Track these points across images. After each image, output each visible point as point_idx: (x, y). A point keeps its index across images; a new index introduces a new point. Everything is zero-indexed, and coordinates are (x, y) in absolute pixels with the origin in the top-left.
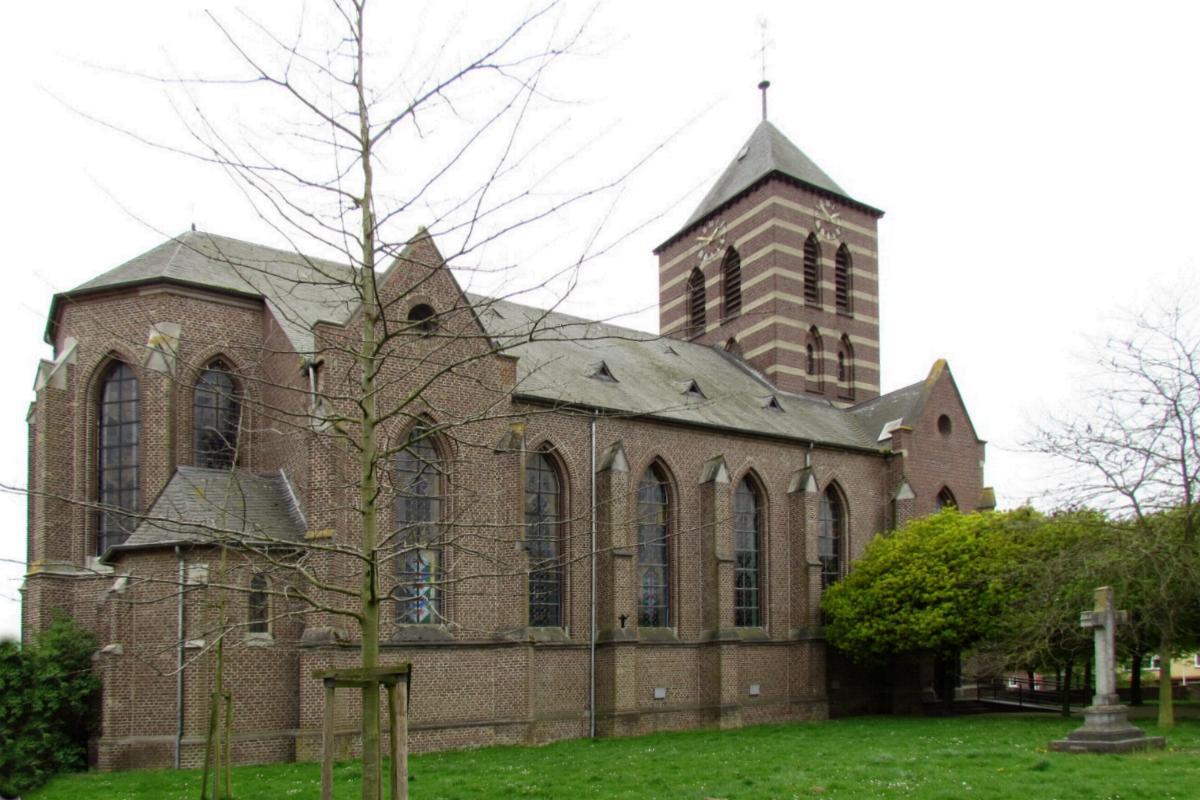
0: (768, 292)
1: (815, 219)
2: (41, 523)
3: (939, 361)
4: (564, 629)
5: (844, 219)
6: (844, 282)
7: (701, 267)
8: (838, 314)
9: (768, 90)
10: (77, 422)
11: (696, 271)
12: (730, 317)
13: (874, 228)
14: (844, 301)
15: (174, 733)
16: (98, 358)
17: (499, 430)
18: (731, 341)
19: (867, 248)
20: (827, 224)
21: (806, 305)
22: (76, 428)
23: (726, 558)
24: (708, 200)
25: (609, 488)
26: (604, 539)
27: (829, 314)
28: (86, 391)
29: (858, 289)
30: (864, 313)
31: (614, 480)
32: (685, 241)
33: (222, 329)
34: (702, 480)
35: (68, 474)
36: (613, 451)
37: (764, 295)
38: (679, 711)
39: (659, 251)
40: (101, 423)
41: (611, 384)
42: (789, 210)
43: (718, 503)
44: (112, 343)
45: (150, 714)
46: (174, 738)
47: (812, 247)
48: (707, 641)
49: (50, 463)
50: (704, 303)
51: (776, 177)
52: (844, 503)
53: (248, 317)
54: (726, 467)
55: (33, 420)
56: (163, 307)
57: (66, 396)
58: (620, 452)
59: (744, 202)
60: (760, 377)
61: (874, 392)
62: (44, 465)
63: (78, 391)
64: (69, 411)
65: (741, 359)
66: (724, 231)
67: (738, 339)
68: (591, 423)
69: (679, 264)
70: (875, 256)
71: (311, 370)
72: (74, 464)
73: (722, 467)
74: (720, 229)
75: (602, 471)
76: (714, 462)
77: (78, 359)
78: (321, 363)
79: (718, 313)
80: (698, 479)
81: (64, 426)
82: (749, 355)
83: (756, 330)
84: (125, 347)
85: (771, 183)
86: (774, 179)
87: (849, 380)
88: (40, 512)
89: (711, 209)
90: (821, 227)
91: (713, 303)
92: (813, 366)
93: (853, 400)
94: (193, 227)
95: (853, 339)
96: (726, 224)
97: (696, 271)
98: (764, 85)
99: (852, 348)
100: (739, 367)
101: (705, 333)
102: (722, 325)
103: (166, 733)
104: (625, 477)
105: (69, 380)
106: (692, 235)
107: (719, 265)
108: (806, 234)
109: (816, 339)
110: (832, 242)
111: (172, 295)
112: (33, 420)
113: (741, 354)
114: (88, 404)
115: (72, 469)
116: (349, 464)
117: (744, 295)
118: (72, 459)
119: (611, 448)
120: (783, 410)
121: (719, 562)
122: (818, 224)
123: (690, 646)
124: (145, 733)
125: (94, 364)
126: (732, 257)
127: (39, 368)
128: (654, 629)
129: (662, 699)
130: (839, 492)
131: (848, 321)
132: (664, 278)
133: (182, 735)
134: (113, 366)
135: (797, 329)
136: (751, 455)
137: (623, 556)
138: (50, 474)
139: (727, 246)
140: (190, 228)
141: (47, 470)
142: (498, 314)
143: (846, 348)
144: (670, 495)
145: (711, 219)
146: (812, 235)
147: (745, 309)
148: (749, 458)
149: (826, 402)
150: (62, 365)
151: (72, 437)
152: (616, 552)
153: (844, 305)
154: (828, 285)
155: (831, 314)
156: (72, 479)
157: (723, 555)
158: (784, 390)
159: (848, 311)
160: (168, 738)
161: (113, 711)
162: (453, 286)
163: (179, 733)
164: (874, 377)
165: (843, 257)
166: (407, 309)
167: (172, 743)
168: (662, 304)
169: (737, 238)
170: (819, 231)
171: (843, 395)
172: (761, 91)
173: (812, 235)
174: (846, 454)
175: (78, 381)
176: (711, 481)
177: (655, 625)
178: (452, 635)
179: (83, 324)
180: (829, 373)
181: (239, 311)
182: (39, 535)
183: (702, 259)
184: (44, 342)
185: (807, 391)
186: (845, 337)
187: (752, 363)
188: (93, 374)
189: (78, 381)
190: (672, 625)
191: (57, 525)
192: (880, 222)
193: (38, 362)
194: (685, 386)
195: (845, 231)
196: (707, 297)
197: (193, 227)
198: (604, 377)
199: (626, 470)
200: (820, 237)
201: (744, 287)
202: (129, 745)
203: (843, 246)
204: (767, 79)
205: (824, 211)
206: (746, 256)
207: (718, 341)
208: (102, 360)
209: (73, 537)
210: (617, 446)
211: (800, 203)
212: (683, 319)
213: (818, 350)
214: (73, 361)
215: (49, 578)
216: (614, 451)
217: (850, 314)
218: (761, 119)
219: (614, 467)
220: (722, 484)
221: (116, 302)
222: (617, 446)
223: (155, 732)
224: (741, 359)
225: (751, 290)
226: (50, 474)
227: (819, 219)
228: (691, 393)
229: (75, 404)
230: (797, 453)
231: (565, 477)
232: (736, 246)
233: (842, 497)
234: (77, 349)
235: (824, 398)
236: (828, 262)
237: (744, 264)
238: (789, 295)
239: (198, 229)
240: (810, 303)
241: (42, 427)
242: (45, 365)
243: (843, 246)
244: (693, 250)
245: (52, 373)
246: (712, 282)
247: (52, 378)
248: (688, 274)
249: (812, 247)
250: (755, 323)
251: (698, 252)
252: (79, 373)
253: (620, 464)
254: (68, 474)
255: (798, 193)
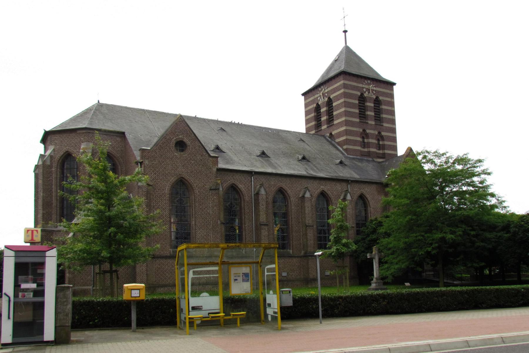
0: (343, 117)
1: (363, 88)
2: (41, 212)
3: (409, 147)
4: (243, 250)
5: (377, 87)
6: (378, 111)
7: (319, 103)
8: (375, 124)
9: (347, 33)
10: (54, 176)
11: (318, 104)
12: (331, 124)
13: (392, 90)
14: (378, 118)
15: (91, 285)
16: (62, 154)
17: (212, 182)
18: (331, 134)
19: (389, 97)
20: (368, 90)
21: (360, 122)
22: (53, 178)
23: (309, 225)
24: (323, 76)
25: (258, 200)
26: (257, 220)
27: (371, 125)
28: (58, 165)
29: (385, 114)
30: (388, 123)
31: (260, 198)
32: (313, 92)
33: (107, 145)
34: (300, 196)
35: (51, 194)
36: (260, 187)
37: (341, 118)
38: (293, 281)
39: (303, 94)
40: (63, 176)
41: (266, 158)
42: (350, 85)
43: (306, 204)
44: (65, 149)
45: (82, 279)
46: (91, 287)
47: (362, 99)
48: (304, 255)
49: (44, 191)
50: (321, 117)
51: (343, 73)
52: (367, 202)
53: (118, 139)
54: (309, 191)
55: (37, 172)
56: (86, 137)
57: (50, 166)
58: (262, 187)
59: (333, 81)
60: (341, 149)
61: (395, 154)
62: (42, 191)
63: (55, 165)
64: (51, 172)
65: (335, 142)
66: (326, 91)
67: (333, 133)
68: (252, 177)
69: (311, 101)
70: (392, 100)
71: (139, 164)
72: (53, 190)
73: (308, 191)
74: (326, 90)
75: (256, 194)
76: (305, 189)
77: (54, 154)
78: (142, 162)
79: (326, 122)
80: (299, 195)
81: (49, 177)
82: (338, 140)
83: (339, 131)
84: (71, 150)
85: (342, 76)
86: (343, 74)
87: (383, 150)
88: (40, 208)
89: (326, 78)
90: (366, 91)
91: (324, 118)
92: (364, 145)
93: (384, 158)
94: (99, 101)
95: (383, 134)
96: (327, 88)
97: (318, 104)
98: (345, 32)
99: (383, 137)
100: (334, 146)
101: (321, 130)
102: (327, 127)
103: (88, 286)
104: (265, 196)
105: (51, 161)
106: (316, 90)
107: (314, 110)
108: (359, 94)
109: (366, 134)
110: (372, 96)
111: (89, 133)
112: (37, 172)
113: (335, 139)
114: (58, 169)
115: (52, 192)
116: (153, 196)
117: (335, 117)
118: (52, 189)
119: (259, 186)
120: (346, 165)
121: (307, 226)
122: (365, 90)
123: (298, 257)
124: (80, 285)
125: (60, 156)
126: (330, 103)
127: (40, 157)
128: (282, 250)
129: (285, 276)
130: (365, 198)
131: (381, 127)
132: (306, 105)
133: (93, 287)
134: (68, 157)
135: (356, 131)
136: (323, 185)
137: (265, 225)
138: (44, 194)
139: (328, 96)
140: (97, 102)
141: (43, 193)
142: (223, 130)
143: (380, 137)
144: (288, 201)
145: (322, 85)
146: (362, 94)
147: (335, 122)
148: (321, 187)
149: (371, 159)
150: (48, 156)
151: (52, 181)
152: (261, 223)
153: (379, 120)
154: (371, 113)
155: (373, 124)
156: (52, 196)
157: (309, 224)
158: (351, 155)
159: (381, 122)
160: (88, 287)
161: (69, 278)
162: (192, 133)
163: (92, 285)
164: (395, 148)
165: (377, 102)
166: (174, 142)
167: (90, 289)
168: (306, 115)
169: (331, 94)
170: (365, 92)
171: (380, 156)
172: (344, 33)
173: (362, 94)
174: (367, 184)
175: (54, 162)
176: (303, 196)
177: (282, 249)
178: (194, 253)
179: (56, 141)
180: (372, 148)
181: (115, 137)
182: (40, 216)
183: (319, 100)
184: (40, 143)
185: (362, 155)
186: (379, 133)
187: (338, 143)
188: (60, 159)
189: (54, 162)
190: (290, 249)
191: (47, 212)
192: (394, 87)
193: (39, 155)
194: (300, 157)
195: (379, 92)
196: (322, 116)
197: (99, 101)
198: (264, 156)
199: (265, 193)
200: (366, 95)
201: (335, 113)
202: (75, 290)
203: (377, 98)
204: (346, 30)
205: (364, 86)
206: (335, 102)
207: (327, 133)
208: (63, 154)
209: (53, 216)
210: (262, 185)
211: (355, 82)
212: (313, 123)
213: (367, 139)
214: (52, 154)
215: (44, 231)
216: (260, 187)
217: (382, 124)
218: (344, 45)
219: (260, 193)
220: (308, 198)
221: (69, 134)
222: (262, 185)
223: (84, 285)
224: (335, 142)
225: (337, 115)
226: (44, 194)
227: (365, 88)
228: (303, 160)
229: (53, 169)
230: (344, 184)
231: (242, 196)
232: (331, 97)
233: (366, 200)
234: (54, 150)
235: (370, 158)
236: (370, 104)
237: (334, 104)
238: (352, 118)
239: (100, 102)
240: (362, 121)
241: (41, 177)
242: (42, 156)
243: (377, 98)
244: (316, 96)
245: (45, 159)
246: (323, 110)
247: (45, 161)
248: (315, 105)
249: (362, 99)
250: (339, 128)
251: (318, 97)
252: (54, 158)
253: (263, 192)
254: (51, 194)
255: (355, 79)
